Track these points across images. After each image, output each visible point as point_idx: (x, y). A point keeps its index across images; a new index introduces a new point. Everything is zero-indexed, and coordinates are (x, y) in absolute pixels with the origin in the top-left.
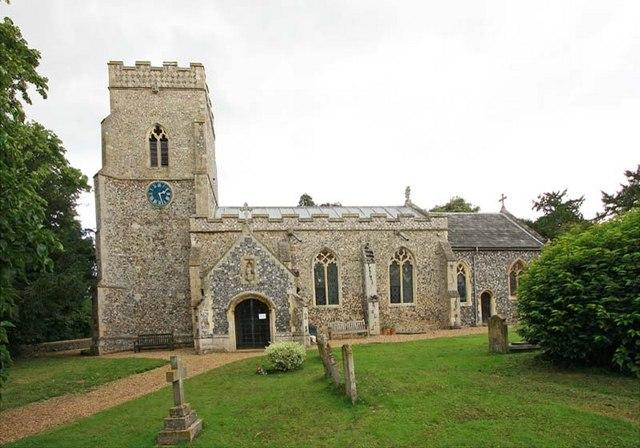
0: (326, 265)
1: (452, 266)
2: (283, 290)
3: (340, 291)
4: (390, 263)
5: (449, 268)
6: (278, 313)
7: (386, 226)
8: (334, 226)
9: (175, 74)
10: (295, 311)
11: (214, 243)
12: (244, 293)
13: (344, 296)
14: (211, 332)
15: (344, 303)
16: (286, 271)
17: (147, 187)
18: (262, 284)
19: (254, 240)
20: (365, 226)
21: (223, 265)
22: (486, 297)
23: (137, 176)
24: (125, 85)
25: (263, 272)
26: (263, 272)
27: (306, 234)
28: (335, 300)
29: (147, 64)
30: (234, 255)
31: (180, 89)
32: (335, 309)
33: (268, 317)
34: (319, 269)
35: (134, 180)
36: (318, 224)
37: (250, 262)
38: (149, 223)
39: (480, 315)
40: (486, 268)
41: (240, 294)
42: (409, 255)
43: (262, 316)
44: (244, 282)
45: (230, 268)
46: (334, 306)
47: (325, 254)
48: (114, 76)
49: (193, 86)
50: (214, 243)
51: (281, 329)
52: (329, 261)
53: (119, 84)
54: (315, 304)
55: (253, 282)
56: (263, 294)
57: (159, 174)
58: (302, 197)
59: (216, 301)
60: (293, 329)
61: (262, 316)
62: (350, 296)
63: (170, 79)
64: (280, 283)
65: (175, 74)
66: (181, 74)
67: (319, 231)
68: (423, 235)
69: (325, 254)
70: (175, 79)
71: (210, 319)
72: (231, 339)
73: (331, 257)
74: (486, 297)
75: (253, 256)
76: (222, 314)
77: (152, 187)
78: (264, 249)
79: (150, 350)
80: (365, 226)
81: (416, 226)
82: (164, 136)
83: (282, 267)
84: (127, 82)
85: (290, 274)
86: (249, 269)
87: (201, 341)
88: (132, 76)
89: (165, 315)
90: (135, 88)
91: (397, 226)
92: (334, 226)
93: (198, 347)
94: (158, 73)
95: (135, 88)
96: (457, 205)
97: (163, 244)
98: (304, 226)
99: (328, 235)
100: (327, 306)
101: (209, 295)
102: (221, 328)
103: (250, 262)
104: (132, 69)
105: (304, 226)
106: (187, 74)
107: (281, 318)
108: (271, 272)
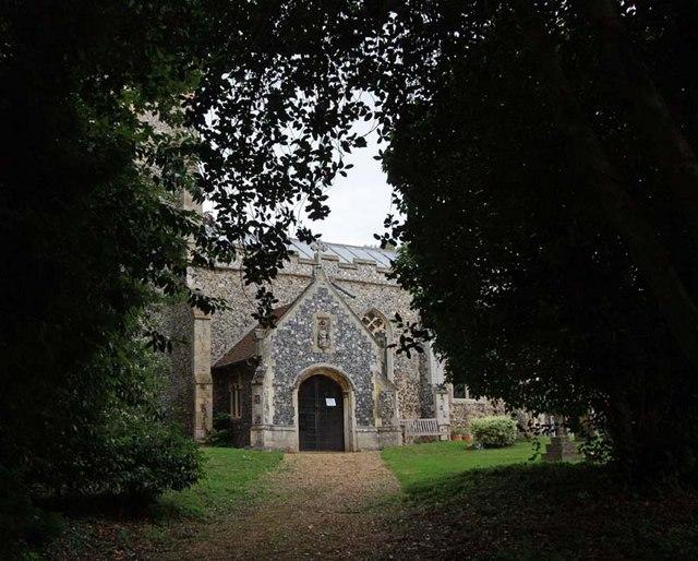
6: (359, 397)
10: (381, 397)
14: (271, 422)
18: (339, 354)
19: (330, 292)
21: (290, 324)
25: (341, 338)
26: (341, 338)
30: (304, 311)
37: (323, 322)
41: (312, 367)
43: (331, 402)
44: (316, 350)
51: (362, 422)
55: (327, 351)
56: (340, 368)
59: (278, 375)
60: (378, 422)
61: (331, 402)
67: (364, 284)
71: (270, 402)
72: (293, 437)
73: (379, 323)
75: (328, 314)
76: (284, 396)
78: (342, 305)
83: (364, 333)
87: (267, 434)
93: (260, 443)
96: (389, 182)
99: (378, 291)
102: (282, 416)
103: (323, 322)
107: (363, 406)
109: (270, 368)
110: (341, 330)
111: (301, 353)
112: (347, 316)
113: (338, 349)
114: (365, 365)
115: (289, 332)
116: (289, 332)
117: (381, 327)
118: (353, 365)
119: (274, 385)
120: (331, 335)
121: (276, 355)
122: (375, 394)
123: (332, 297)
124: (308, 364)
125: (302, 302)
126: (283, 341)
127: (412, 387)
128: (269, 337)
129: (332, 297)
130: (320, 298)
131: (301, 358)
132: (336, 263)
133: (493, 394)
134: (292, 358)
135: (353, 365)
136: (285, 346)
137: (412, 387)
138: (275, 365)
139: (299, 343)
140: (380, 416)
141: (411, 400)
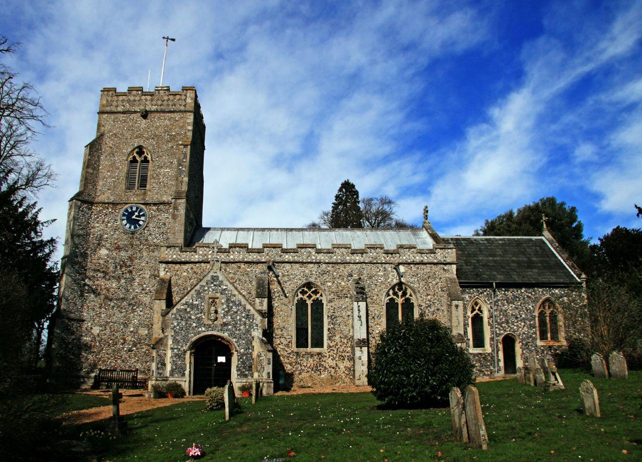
0: (309, 302)
1: (457, 306)
2: (248, 331)
3: (326, 333)
4: (387, 300)
5: (453, 308)
6: (241, 356)
7: (383, 258)
8: (321, 257)
9: (166, 98)
10: (259, 356)
11: (185, 274)
12: (204, 332)
13: (330, 338)
15: (329, 347)
16: (253, 311)
17: (122, 211)
18: (225, 324)
19: (221, 278)
20: (358, 258)
21: (186, 303)
22: (509, 343)
23: (112, 199)
24: (114, 109)
27: (288, 266)
28: (318, 343)
29: (140, 89)
30: (198, 293)
31: (170, 112)
32: (319, 354)
33: (229, 360)
34: (301, 305)
35: (108, 203)
36: (303, 256)
38: (118, 248)
39: (502, 364)
40: (510, 308)
41: (202, 334)
42: (409, 291)
43: (222, 359)
45: (192, 306)
46: (317, 350)
47: (309, 288)
48: (105, 102)
49: (182, 108)
50: (185, 274)
52: (314, 297)
53: (108, 109)
54: (294, 345)
56: (226, 335)
57: (134, 197)
58: (342, 184)
59: (175, 341)
61: (222, 359)
62: (337, 338)
63: (160, 102)
64: (245, 324)
65: (166, 98)
66: (171, 97)
67: (303, 263)
68: (427, 269)
69: (309, 288)
70: (165, 103)
73: (316, 292)
74: (509, 343)
75: (218, 295)
76: (180, 356)
77: (126, 211)
78: (230, 287)
79: (296, 312)
80: (358, 258)
81: (418, 258)
82: (146, 157)
83: (248, 307)
84: (117, 106)
85: (257, 316)
86: (213, 308)
88: (123, 101)
89: (123, 353)
90: (124, 113)
91: (396, 259)
92: (321, 257)
94: (149, 98)
95: (124, 113)
97: (131, 272)
98: (287, 257)
100: (309, 349)
101: (170, 333)
104: (124, 94)
105: (287, 257)
106: (178, 97)
107: (243, 363)
108: (236, 312)
109: (170, 337)
110: (228, 306)
111: (194, 325)
112: (234, 296)
113: (225, 320)
114: (248, 331)
115: (186, 310)
116: (186, 310)
117: (318, 296)
118: (237, 332)
119: (171, 348)
120: (219, 310)
121: (175, 327)
122: (255, 354)
123: (222, 282)
124: (199, 333)
125: (197, 287)
126: (180, 316)
127: (345, 341)
128: (170, 314)
129: (222, 282)
130: (212, 283)
131: (193, 329)
132: (279, 250)
133: (278, 391)
134: (188, 328)
135: (237, 332)
136: (182, 320)
137: (345, 341)
138: (173, 334)
139: (193, 317)
140: (257, 371)
141: (344, 351)
